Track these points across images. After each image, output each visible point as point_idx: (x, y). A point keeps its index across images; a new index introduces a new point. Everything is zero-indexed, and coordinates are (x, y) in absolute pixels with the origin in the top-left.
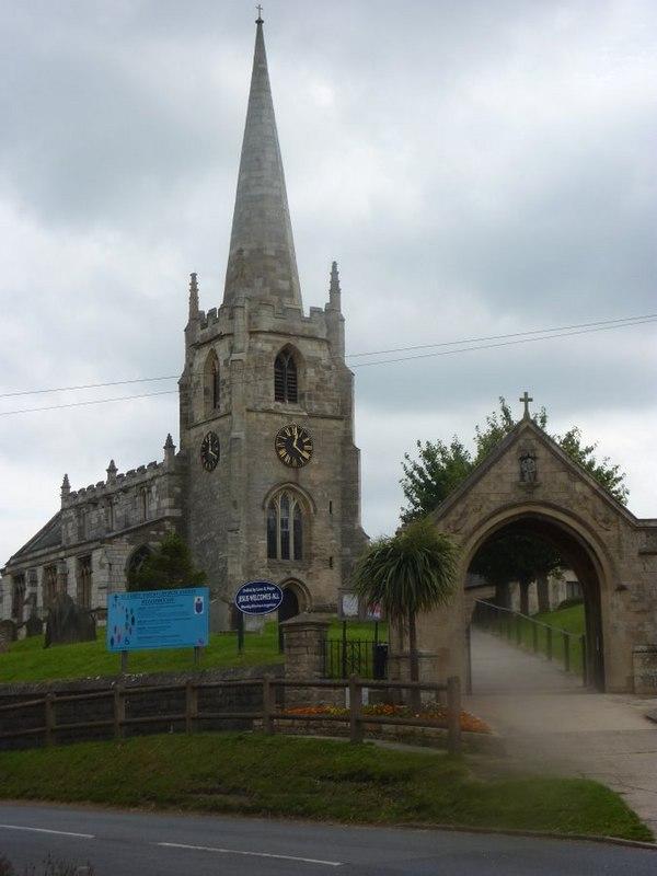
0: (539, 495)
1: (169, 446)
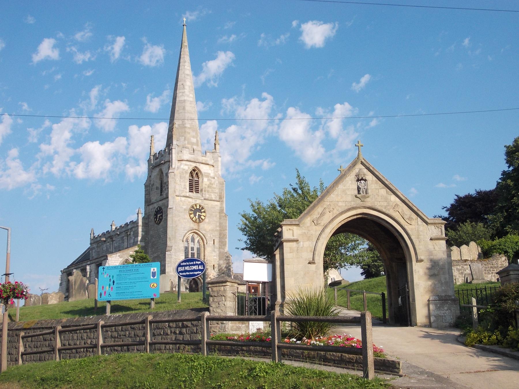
0: (369, 202)
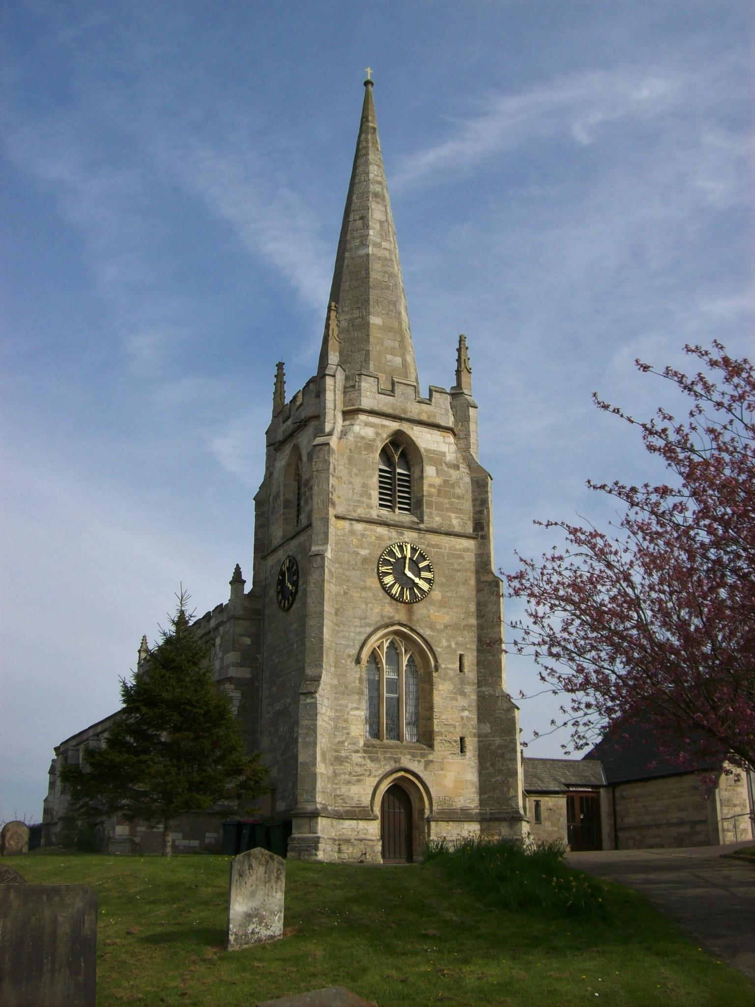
1: (237, 580)
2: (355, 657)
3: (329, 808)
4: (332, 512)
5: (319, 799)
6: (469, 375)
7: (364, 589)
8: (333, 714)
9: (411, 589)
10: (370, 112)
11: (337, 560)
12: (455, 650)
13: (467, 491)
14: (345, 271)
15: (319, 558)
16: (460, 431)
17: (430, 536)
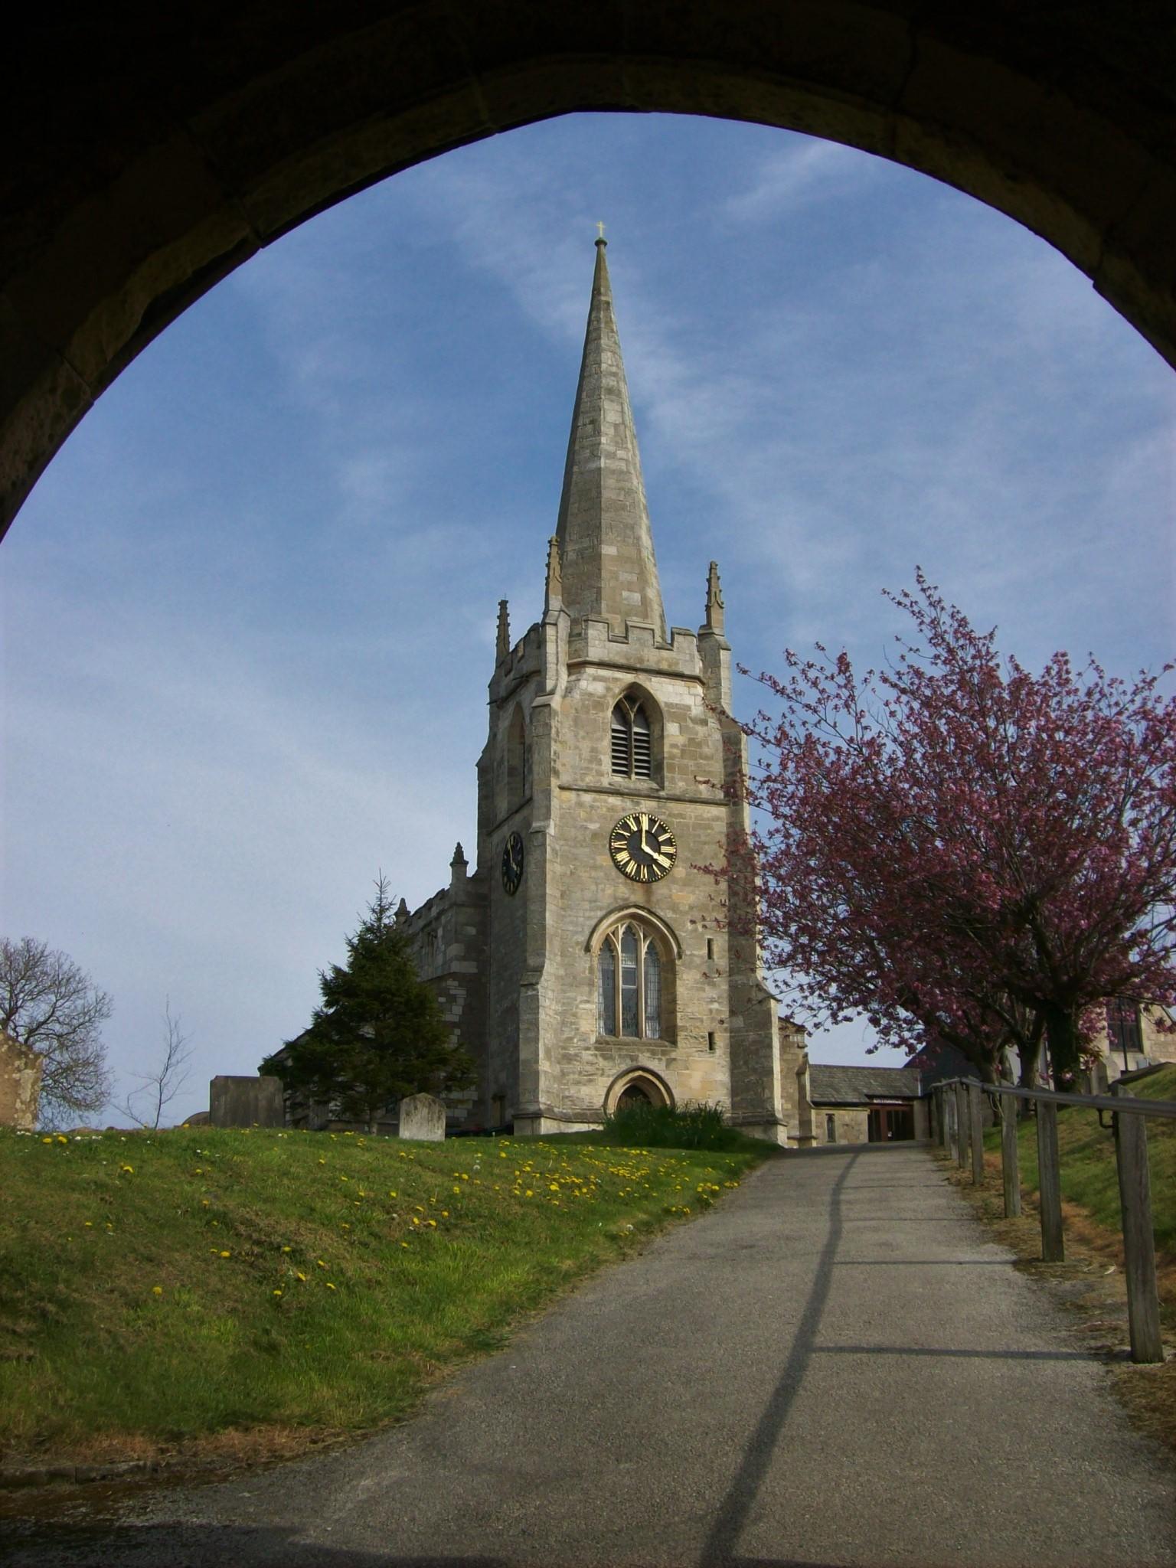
1: (459, 861)
2: (585, 944)
3: (556, 1110)
4: (554, 782)
5: (542, 1099)
6: (721, 610)
7: (595, 867)
8: (559, 1008)
9: (650, 867)
10: (603, 282)
11: (561, 836)
12: (702, 934)
13: (717, 750)
14: (573, 489)
15: (540, 835)
16: (710, 678)
17: (672, 805)
